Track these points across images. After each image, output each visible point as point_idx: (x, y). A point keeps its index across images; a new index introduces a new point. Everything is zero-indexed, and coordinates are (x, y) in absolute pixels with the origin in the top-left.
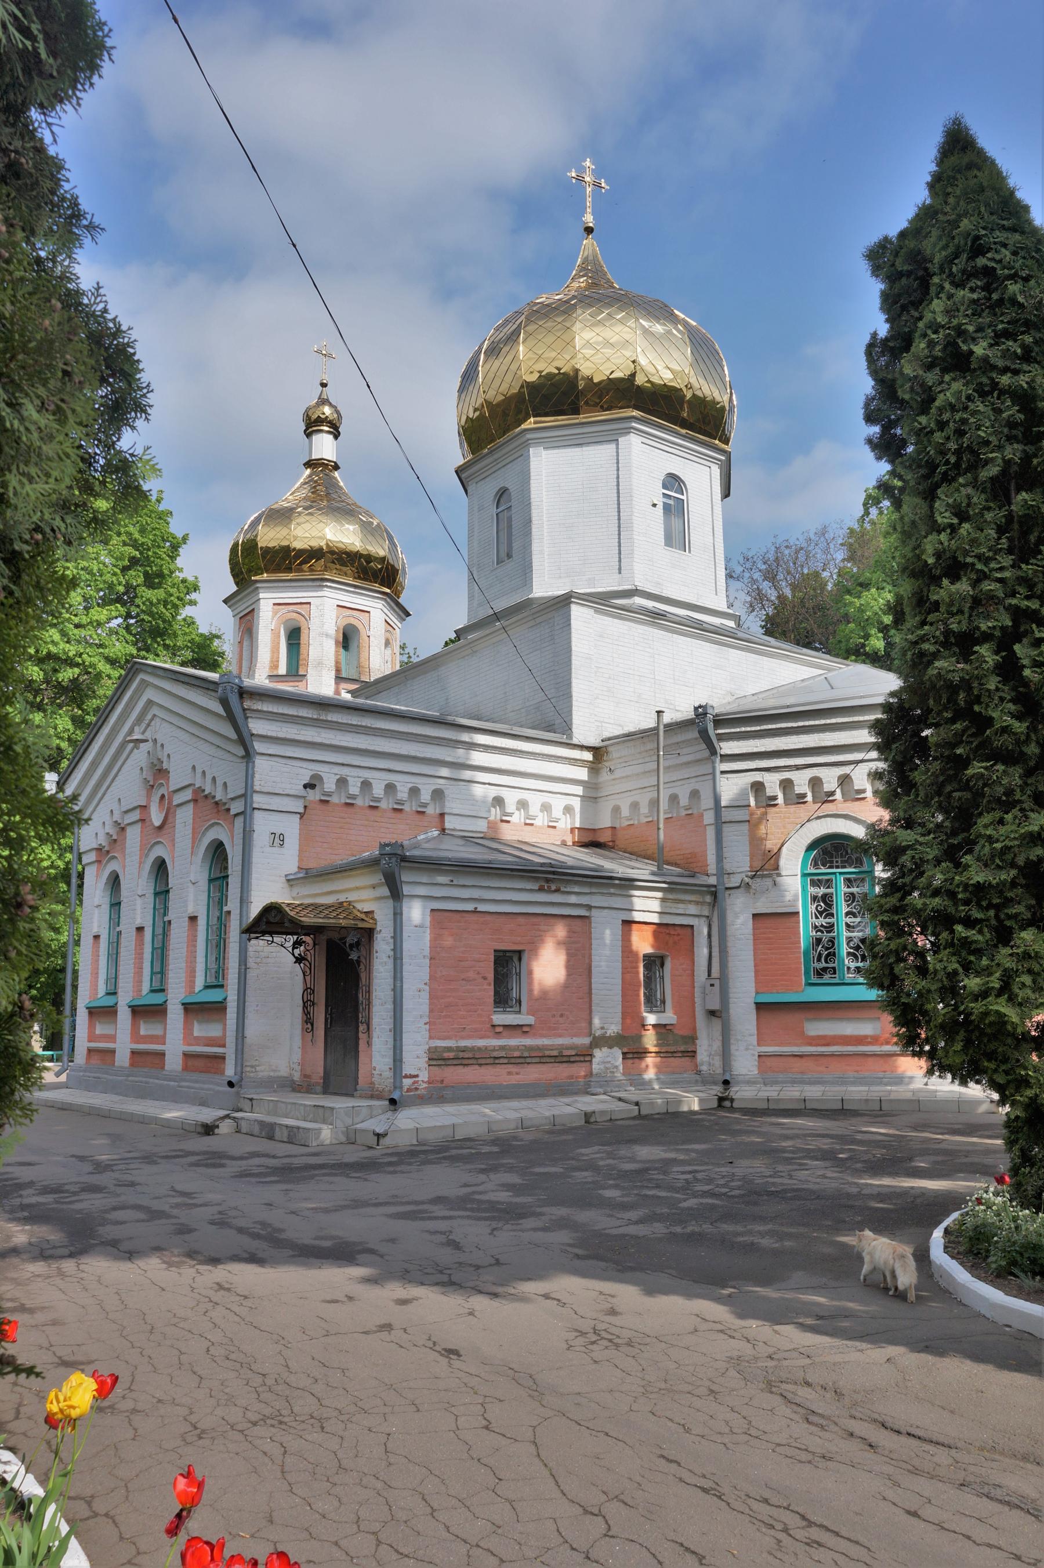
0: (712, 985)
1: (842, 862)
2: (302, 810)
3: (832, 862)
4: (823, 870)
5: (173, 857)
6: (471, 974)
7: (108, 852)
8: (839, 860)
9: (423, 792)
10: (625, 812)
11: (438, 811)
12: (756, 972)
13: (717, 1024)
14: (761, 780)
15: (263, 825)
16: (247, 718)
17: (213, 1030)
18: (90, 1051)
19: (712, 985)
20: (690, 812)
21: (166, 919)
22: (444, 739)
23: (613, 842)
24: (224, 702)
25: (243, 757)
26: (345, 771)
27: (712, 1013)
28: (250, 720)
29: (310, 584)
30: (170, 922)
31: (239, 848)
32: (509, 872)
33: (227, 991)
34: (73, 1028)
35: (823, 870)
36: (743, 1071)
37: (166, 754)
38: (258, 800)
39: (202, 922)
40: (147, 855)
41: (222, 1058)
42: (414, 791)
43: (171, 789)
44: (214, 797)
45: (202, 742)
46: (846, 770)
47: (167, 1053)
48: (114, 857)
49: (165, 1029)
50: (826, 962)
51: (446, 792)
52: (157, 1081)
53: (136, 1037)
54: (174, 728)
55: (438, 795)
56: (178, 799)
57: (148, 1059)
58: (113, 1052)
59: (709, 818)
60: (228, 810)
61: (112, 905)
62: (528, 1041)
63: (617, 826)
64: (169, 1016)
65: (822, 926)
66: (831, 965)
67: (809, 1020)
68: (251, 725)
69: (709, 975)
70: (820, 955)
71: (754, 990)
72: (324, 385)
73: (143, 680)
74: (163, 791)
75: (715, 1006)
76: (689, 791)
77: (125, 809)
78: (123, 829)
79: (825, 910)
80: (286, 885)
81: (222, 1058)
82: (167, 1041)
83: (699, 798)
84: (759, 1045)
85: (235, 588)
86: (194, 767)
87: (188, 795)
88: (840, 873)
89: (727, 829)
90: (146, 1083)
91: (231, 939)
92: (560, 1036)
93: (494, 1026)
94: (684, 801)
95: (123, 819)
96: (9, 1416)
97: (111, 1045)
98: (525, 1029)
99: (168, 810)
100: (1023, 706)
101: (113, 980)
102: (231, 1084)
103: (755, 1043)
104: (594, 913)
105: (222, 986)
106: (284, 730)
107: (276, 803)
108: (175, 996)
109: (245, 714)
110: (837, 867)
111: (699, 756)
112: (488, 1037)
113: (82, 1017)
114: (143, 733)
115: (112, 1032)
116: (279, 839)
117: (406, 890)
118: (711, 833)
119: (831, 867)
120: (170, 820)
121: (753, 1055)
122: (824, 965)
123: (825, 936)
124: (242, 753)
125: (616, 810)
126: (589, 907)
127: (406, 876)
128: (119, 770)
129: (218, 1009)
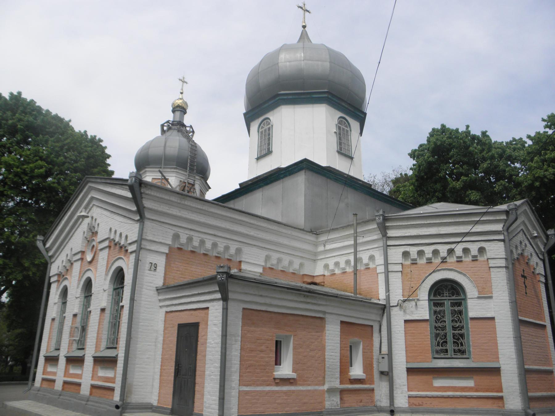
0: (383, 358)
1: (449, 294)
2: (167, 251)
3: (443, 294)
4: (439, 298)
5: (95, 277)
6: (263, 348)
9: (231, 248)
10: (331, 267)
12: (406, 351)
16: (142, 198)
17: (109, 374)
19: (383, 358)
22: (244, 221)
23: (324, 282)
26: (192, 233)
27: (382, 373)
28: (144, 199)
30: (90, 312)
31: (131, 271)
32: (286, 290)
33: (118, 351)
35: (439, 298)
36: (400, 405)
37: (97, 223)
39: (108, 312)
40: (82, 277)
41: (112, 389)
44: (120, 244)
46: (453, 246)
47: (82, 384)
48: (66, 278)
49: (115, 373)
50: (442, 346)
51: (243, 249)
52: (75, 400)
53: (66, 373)
55: (239, 251)
57: (72, 386)
58: (54, 381)
59: (381, 269)
60: (127, 250)
62: (292, 388)
64: (85, 363)
65: (439, 327)
66: (444, 348)
67: (434, 378)
69: (380, 352)
70: (439, 343)
73: (90, 187)
75: (386, 369)
76: (369, 255)
77: (73, 253)
78: (72, 264)
80: (156, 292)
81: (112, 389)
82: (83, 377)
84: (408, 391)
86: (111, 229)
88: (449, 300)
89: (391, 275)
90: (70, 400)
91: (123, 321)
92: (309, 385)
93: (275, 379)
98: (292, 381)
101: (59, 342)
102: (117, 407)
103: (407, 390)
104: (327, 317)
105: (116, 348)
107: (154, 247)
108: (89, 353)
109: (141, 196)
110: (446, 296)
111: (375, 237)
112: (271, 385)
114: (88, 213)
117: (231, 295)
118: (381, 279)
119: (443, 296)
120: (95, 258)
121: (405, 396)
123: (442, 333)
126: (324, 313)
127: (231, 288)
128: (73, 234)
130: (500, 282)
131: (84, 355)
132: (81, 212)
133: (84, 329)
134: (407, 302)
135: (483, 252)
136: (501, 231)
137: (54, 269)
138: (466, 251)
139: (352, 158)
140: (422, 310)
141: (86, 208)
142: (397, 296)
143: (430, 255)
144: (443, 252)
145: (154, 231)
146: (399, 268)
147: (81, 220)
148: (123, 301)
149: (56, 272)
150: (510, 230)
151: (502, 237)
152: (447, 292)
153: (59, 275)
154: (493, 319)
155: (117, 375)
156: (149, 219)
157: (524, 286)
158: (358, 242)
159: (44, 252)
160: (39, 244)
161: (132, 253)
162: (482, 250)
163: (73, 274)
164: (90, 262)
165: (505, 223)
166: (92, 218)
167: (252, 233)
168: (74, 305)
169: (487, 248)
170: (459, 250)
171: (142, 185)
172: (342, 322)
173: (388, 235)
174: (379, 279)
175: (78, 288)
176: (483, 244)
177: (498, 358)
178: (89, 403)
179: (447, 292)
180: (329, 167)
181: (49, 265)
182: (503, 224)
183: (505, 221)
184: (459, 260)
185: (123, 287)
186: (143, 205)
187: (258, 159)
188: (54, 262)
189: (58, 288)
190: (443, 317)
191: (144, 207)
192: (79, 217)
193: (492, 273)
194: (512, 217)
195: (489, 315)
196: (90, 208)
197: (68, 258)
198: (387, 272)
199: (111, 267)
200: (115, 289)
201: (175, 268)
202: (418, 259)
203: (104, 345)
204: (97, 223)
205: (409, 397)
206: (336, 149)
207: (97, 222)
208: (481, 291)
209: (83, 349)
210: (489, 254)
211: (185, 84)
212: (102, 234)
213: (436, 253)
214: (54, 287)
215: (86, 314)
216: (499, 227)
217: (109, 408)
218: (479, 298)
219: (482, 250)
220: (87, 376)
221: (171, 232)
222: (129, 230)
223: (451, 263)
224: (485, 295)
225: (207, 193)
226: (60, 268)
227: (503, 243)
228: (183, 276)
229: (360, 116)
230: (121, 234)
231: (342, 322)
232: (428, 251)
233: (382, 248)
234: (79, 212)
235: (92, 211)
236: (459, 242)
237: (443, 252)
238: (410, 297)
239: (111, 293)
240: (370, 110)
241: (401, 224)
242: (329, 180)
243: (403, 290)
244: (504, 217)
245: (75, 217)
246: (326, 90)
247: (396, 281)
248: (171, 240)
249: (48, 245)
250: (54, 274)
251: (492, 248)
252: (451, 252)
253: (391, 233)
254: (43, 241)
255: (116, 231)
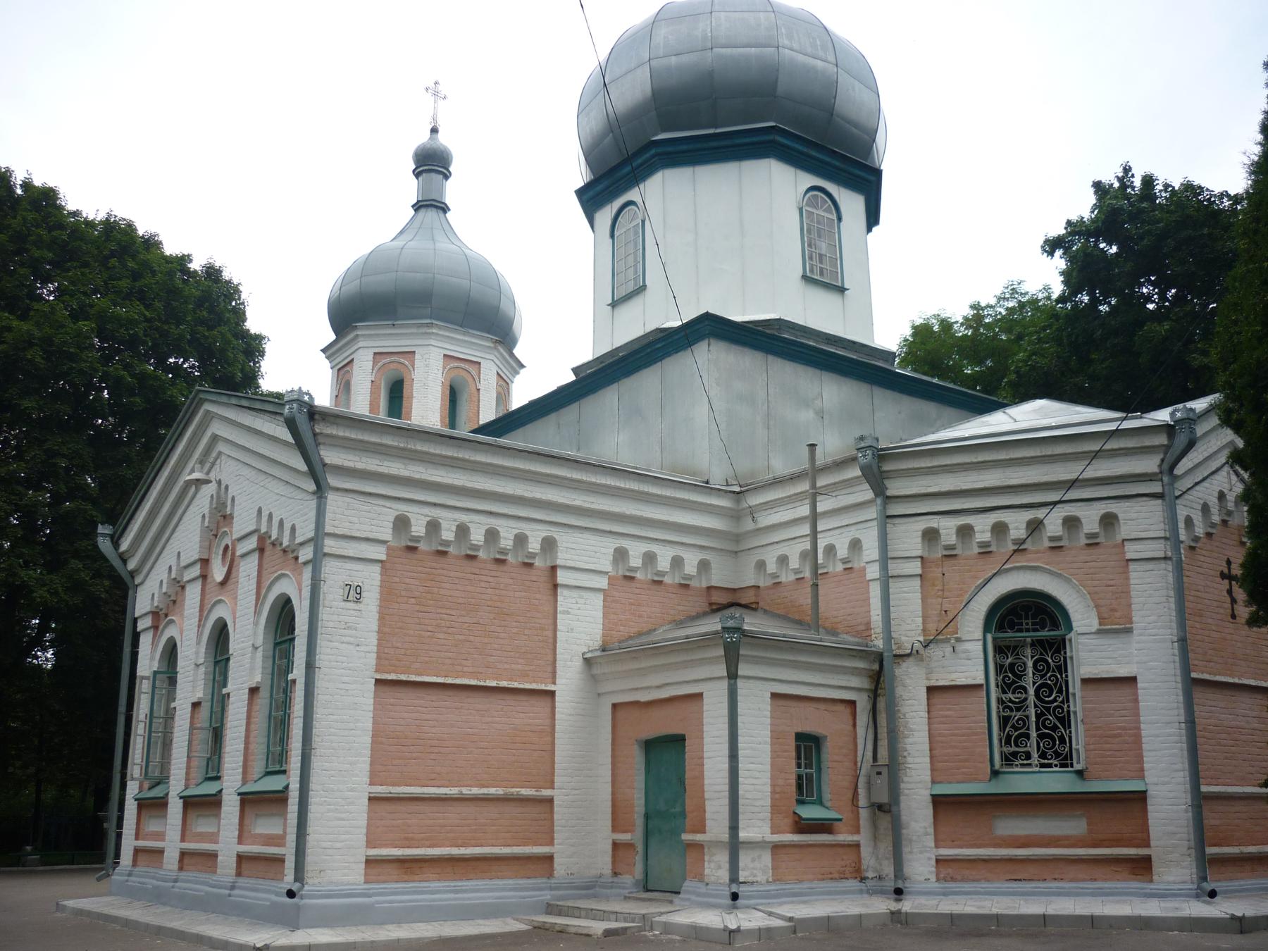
0: (879, 773)
5: (235, 618)
7: (166, 615)
8: (1030, 621)
10: (771, 567)
11: (549, 564)
13: (884, 822)
14: (935, 525)
15: (335, 575)
16: (318, 444)
18: (137, 851)
19: (879, 773)
20: (849, 566)
21: (225, 691)
24: (291, 424)
25: (314, 493)
27: (880, 808)
29: (414, 330)
31: (306, 603)
34: (120, 824)
38: (330, 545)
41: (280, 860)
42: (521, 540)
43: (234, 537)
45: (270, 479)
46: (1040, 513)
48: (172, 621)
54: (240, 465)
55: (549, 545)
56: (242, 549)
59: (873, 572)
60: (297, 558)
61: (216, 663)
63: (761, 584)
64: (224, 809)
65: (1011, 701)
68: (322, 453)
71: (928, 779)
72: (435, 91)
73: (208, 412)
74: (227, 541)
75: (884, 798)
77: (183, 564)
78: (183, 587)
79: (1014, 682)
81: (280, 860)
83: (860, 548)
84: (937, 846)
85: (333, 337)
86: (260, 511)
87: (252, 543)
89: (894, 586)
94: (842, 552)
95: (182, 575)
96: (497, 905)
97: (158, 844)
99: (232, 561)
100: (1247, 443)
105: (284, 772)
106: (364, 459)
108: (231, 783)
110: (1028, 630)
113: (131, 808)
114: (208, 473)
115: (212, 829)
116: (355, 593)
118: (875, 591)
119: (1021, 631)
120: (233, 575)
121: (929, 859)
122: (1014, 749)
124: (313, 487)
125: (761, 565)
129: (279, 798)
130: (1151, 594)
131: (221, 791)
132: (193, 471)
133: (217, 735)
134: (932, 646)
135: (1112, 524)
136: (1155, 474)
137: (144, 601)
138: (1071, 523)
139: (841, 290)
140: (969, 662)
141: (202, 462)
142: (909, 630)
143: (986, 537)
144: (1017, 528)
145: (345, 513)
146: (915, 567)
147: (193, 488)
148: (295, 671)
149: (148, 609)
150: (1179, 470)
151: (1156, 488)
152: (1027, 624)
153: (155, 614)
154: (1133, 680)
155: (289, 830)
156: (338, 489)
157: (1228, 599)
158: (819, 510)
159: (116, 563)
160: (105, 545)
161: (305, 563)
162: (1109, 521)
163: (186, 613)
164: (223, 583)
165: (1166, 454)
166: (219, 483)
167: (579, 500)
168: (192, 684)
169: (1120, 516)
170: (1053, 523)
171: (317, 417)
172: (775, 696)
173: (889, 493)
174: (872, 594)
175: (198, 643)
176: (1113, 507)
177: (1142, 770)
178: (236, 892)
179: (1027, 624)
180: (780, 323)
181: (131, 592)
182: (1161, 456)
183: (1167, 448)
184: (1056, 548)
185: (293, 639)
186: (322, 460)
187: (614, 304)
188: (142, 583)
189: (154, 643)
190: (1020, 677)
191: (325, 465)
192: (188, 484)
193: (1133, 575)
194: (1181, 440)
195: (1123, 672)
196: (211, 460)
197: (173, 576)
198: (886, 579)
199: (265, 597)
200: (276, 644)
201: (403, 593)
202: (959, 546)
203: (258, 766)
204: (230, 497)
205: (937, 861)
206: (801, 272)
207: (231, 493)
208: (1106, 615)
209: (218, 778)
210: (1125, 531)
211: (441, 102)
212: (243, 522)
213: (1000, 529)
214: (145, 642)
215: (220, 702)
216: (1150, 464)
217: (274, 898)
218: (1099, 632)
219: (1109, 521)
220: (226, 834)
221: (389, 513)
222: (292, 510)
223: (1037, 552)
224: (1116, 624)
225: (517, 379)
226: (165, 585)
227: (1159, 502)
228: (423, 609)
229: (867, 181)
230: (281, 523)
231: (775, 696)
232: (982, 526)
233: (875, 523)
234: (188, 469)
235: (217, 467)
236: (1055, 503)
237: (1017, 528)
238: (941, 633)
239: (271, 653)
240: (896, 161)
241: (910, 466)
242: (770, 358)
243: (925, 617)
244: (1162, 439)
245: (180, 483)
246: (772, 124)
247: (909, 599)
248: (390, 531)
249: (124, 546)
250: (144, 611)
251: (1135, 515)
252: (1035, 527)
253: (896, 487)
254: (112, 537)
255: (270, 516)
